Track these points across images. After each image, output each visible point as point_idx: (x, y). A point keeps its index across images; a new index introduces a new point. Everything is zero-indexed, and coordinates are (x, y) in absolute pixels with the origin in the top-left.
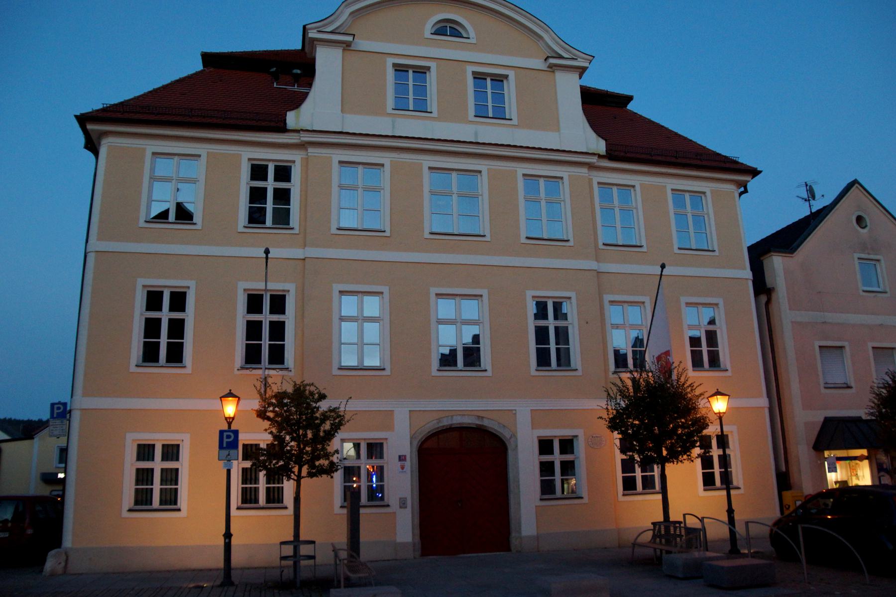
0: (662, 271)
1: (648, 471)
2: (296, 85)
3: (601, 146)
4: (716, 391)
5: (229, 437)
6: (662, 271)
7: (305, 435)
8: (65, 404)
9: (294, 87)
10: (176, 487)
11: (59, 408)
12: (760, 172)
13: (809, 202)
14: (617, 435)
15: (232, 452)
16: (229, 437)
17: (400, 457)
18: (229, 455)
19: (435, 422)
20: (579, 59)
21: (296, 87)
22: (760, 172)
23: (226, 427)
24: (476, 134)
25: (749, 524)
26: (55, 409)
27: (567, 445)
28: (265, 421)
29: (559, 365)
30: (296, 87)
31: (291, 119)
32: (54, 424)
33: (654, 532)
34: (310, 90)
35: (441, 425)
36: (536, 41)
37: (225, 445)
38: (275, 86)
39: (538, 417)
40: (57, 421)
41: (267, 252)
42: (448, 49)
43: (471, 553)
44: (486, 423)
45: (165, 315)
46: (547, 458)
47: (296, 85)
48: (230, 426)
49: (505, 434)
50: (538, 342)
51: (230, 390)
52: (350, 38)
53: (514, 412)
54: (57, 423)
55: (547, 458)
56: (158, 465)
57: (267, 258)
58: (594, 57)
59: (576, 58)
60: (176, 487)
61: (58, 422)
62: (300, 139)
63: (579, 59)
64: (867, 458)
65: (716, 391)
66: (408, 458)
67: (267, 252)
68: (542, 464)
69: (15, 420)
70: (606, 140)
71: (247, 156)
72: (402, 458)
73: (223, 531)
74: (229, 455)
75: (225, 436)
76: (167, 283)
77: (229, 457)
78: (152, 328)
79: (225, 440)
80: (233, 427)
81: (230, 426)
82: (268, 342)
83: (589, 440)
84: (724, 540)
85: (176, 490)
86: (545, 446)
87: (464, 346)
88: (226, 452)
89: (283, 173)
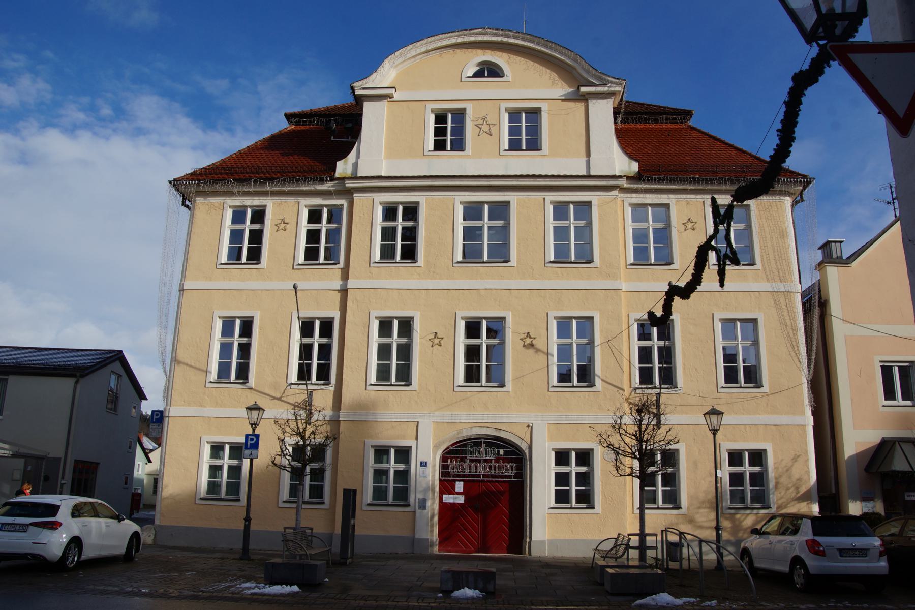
2: (350, 137)
4: (712, 408)
5: (252, 439)
8: (162, 412)
9: (348, 138)
11: (157, 415)
13: (894, 205)
14: (242, 440)
15: (254, 452)
16: (252, 439)
17: (421, 463)
19: (456, 432)
21: (350, 139)
23: (251, 432)
25: (655, 537)
26: (155, 415)
29: (488, 381)
30: (350, 139)
31: (343, 168)
33: (616, 542)
35: (461, 435)
38: (332, 139)
39: (557, 428)
42: (489, 88)
44: (503, 435)
45: (316, 340)
46: (563, 469)
47: (350, 137)
48: (254, 431)
50: (380, 358)
51: (256, 402)
55: (563, 469)
56: (574, 469)
57: (296, 289)
61: (156, 425)
65: (712, 408)
66: (430, 465)
68: (558, 475)
71: (306, 204)
72: (423, 464)
73: (244, 515)
75: (249, 439)
76: (395, 312)
80: (257, 432)
81: (254, 431)
83: (605, 453)
84: (715, 560)
86: (562, 457)
87: (882, 364)
89: (411, 212)
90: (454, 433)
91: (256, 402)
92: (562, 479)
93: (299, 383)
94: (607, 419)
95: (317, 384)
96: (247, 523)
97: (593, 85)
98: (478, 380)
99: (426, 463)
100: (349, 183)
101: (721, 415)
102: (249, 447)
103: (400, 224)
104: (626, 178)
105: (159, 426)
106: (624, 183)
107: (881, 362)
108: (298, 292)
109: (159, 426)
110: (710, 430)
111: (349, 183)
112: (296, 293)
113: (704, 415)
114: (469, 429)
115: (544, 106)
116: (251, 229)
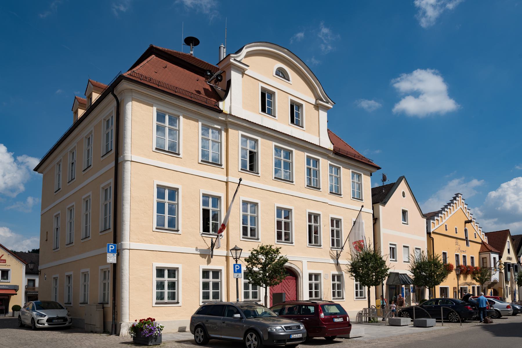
0: (240, 182)
5: (237, 267)
6: (240, 182)
7: (362, 270)
12: (381, 168)
15: (239, 274)
18: (238, 275)
20: (329, 104)
22: (381, 168)
27: (173, 272)
28: (24, 252)
31: (223, 106)
32: (110, 255)
36: (145, 101)
37: (236, 271)
40: (111, 254)
41: (240, 180)
43: (289, 342)
54: (111, 255)
55: (216, 280)
63: (329, 104)
64: (369, 288)
67: (240, 180)
69: (36, 250)
74: (238, 275)
77: (238, 276)
79: (236, 269)
82: (167, 215)
86: (310, 276)
88: (236, 274)
101: (240, 251)
105: (114, 255)
107: (390, 244)
109: (114, 255)
110: (234, 259)
112: (239, 185)
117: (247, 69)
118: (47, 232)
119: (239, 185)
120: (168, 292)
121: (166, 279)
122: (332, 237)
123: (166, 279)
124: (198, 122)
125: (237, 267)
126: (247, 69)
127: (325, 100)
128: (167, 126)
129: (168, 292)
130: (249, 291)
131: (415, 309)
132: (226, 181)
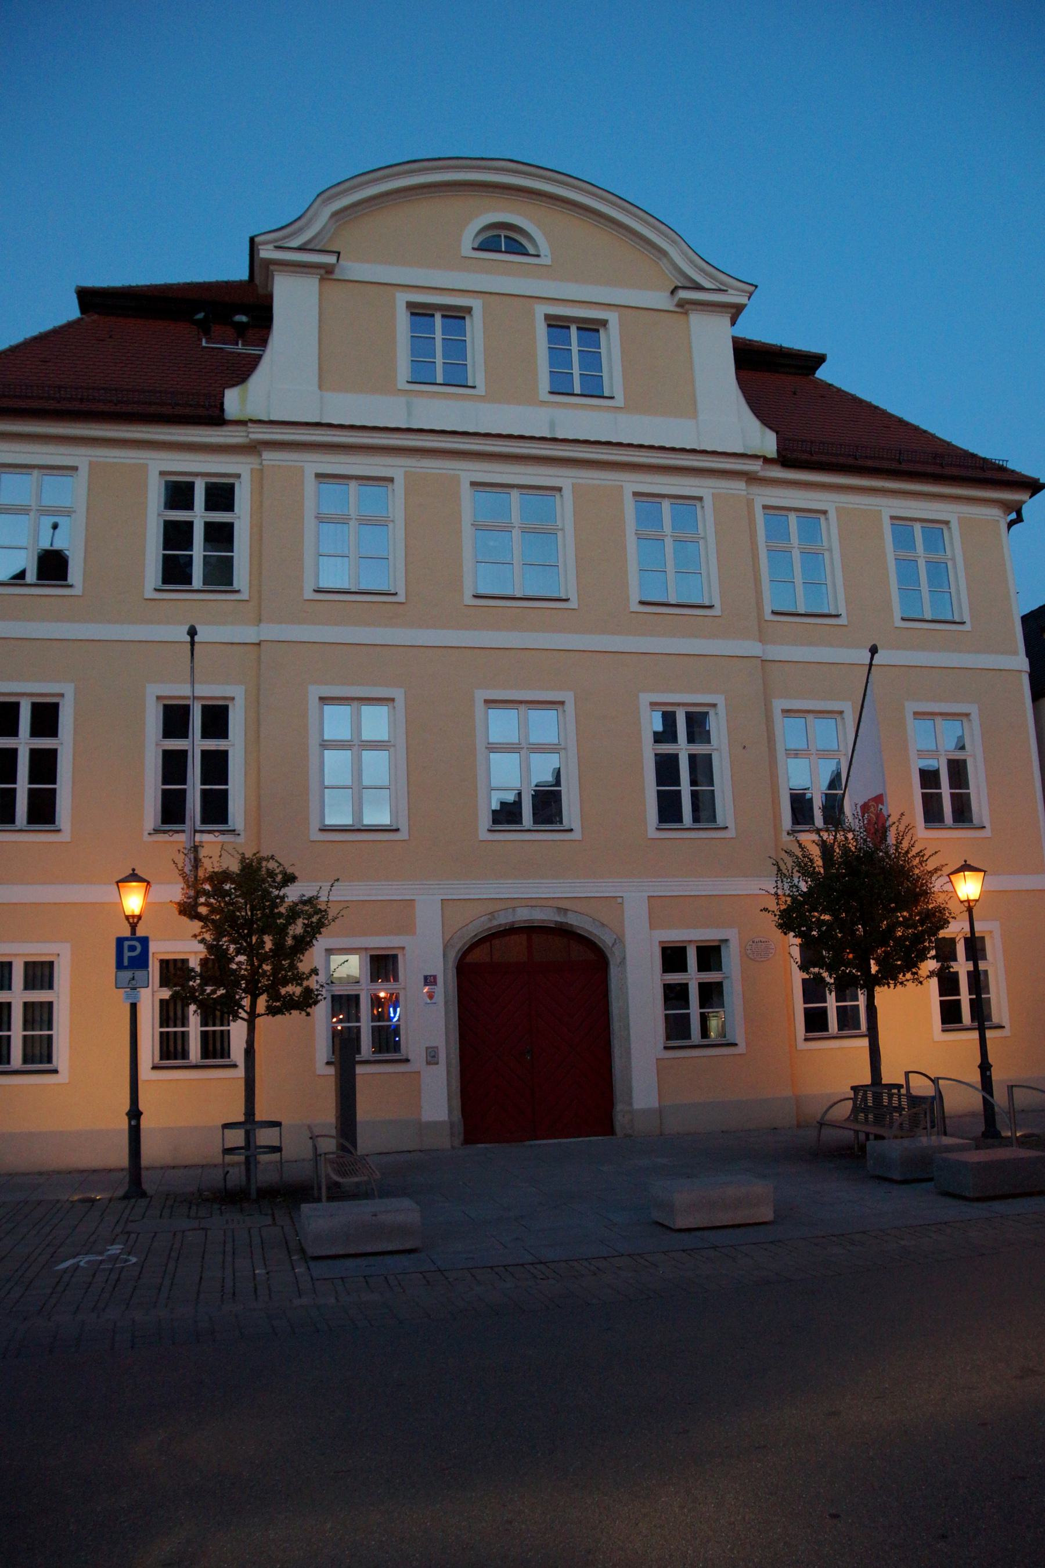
0: (872, 659)
1: (848, 998)
2: (240, 342)
3: (767, 443)
5: (132, 948)
6: (872, 659)
10: (358, 1024)
15: (139, 974)
17: (426, 978)
18: (133, 979)
20: (731, 291)
21: (240, 346)
24: (552, 426)
29: (696, 819)
31: (233, 401)
33: (855, 1104)
34: (263, 350)
35: (495, 923)
37: (126, 963)
38: (204, 344)
41: (874, 650)
44: (572, 920)
49: (604, 938)
52: (331, 259)
53: (619, 900)
58: (756, 287)
59: (725, 288)
60: (358, 1024)
62: (247, 436)
63: (731, 291)
70: (777, 433)
72: (429, 980)
73: (127, 1107)
74: (133, 979)
77: (134, 982)
78: (666, 769)
79: (127, 954)
80: (140, 932)
82: (199, 787)
85: (50, 1037)
90: (482, 919)
91: (965, 861)
92: (675, 995)
93: (695, 827)
94: (305, 888)
95: (165, 832)
96: (133, 1123)
97: (699, 288)
98: (679, 819)
99: (435, 977)
100: (253, 432)
102: (126, 963)
103: (199, 516)
104: (762, 459)
106: (755, 466)
108: (196, 647)
111: (253, 432)
112: (870, 669)
113: (117, 883)
114: (511, 910)
115: (613, 317)
116: (208, 520)
117: (745, 305)
118: (947, 865)
119: (870, 669)
120: (837, 1007)
121: (693, 977)
122: (922, 788)
123: (693, 977)
124: (261, 456)
125: (132, 948)
126: (745, 305)
127: (707, 284)
128: (667, 536)
129: (837, 1007)
130: (372, 1022)
131: (168, 1059)
132: (257, 642)
